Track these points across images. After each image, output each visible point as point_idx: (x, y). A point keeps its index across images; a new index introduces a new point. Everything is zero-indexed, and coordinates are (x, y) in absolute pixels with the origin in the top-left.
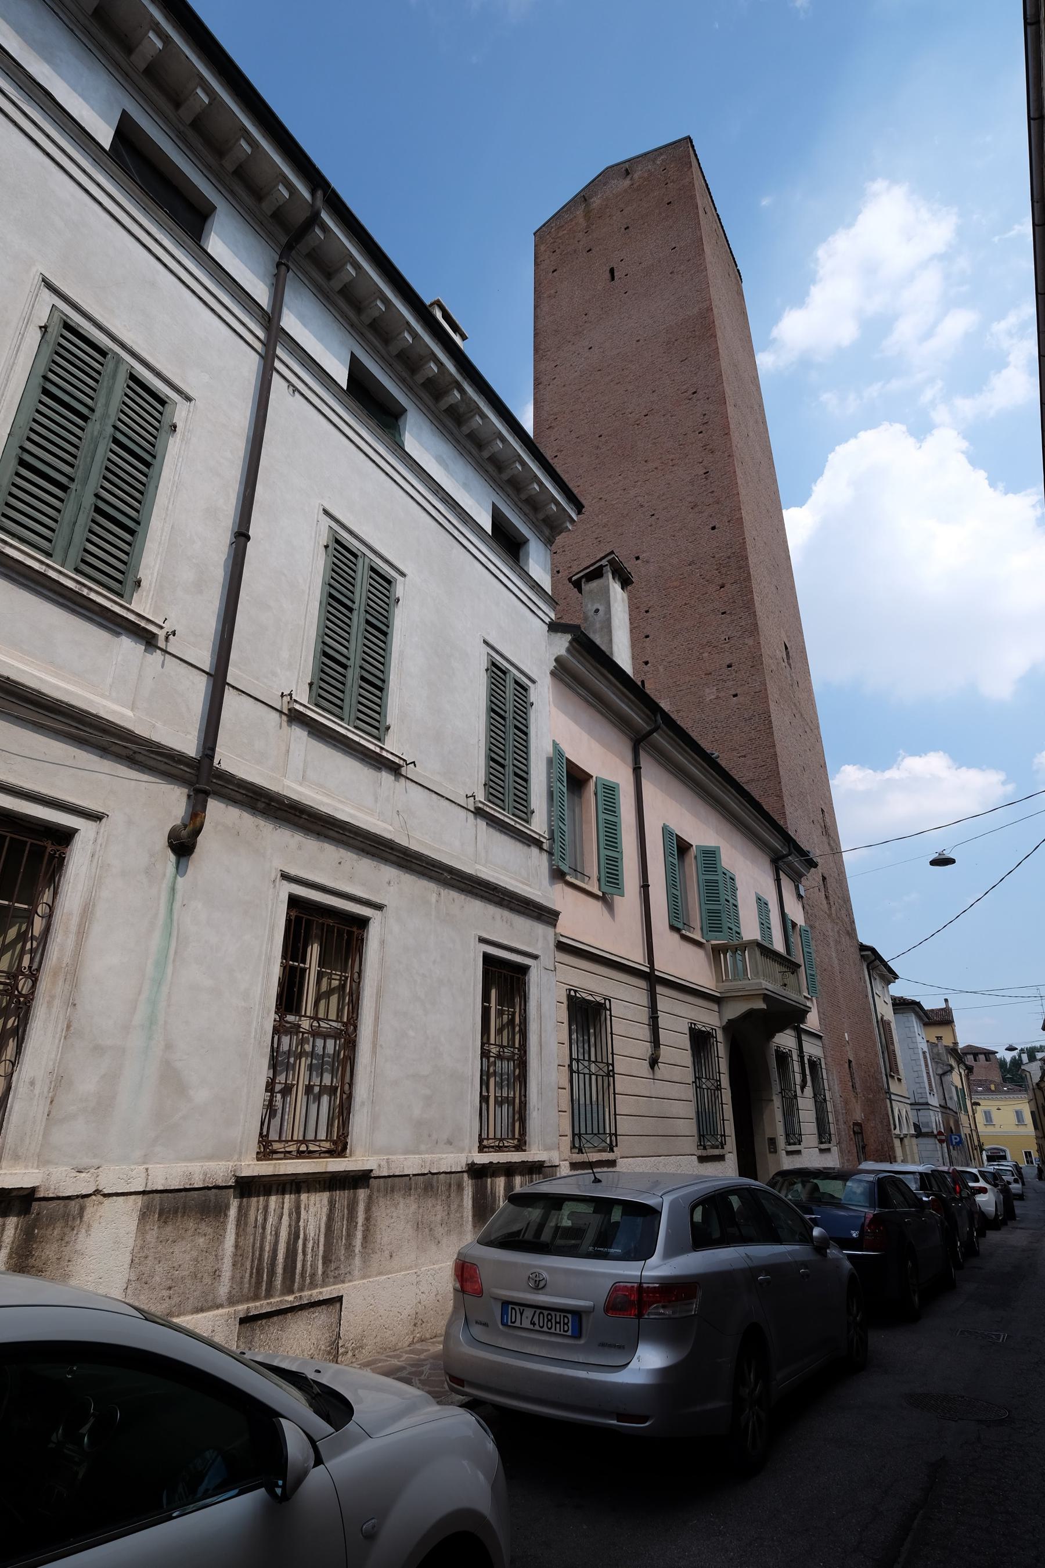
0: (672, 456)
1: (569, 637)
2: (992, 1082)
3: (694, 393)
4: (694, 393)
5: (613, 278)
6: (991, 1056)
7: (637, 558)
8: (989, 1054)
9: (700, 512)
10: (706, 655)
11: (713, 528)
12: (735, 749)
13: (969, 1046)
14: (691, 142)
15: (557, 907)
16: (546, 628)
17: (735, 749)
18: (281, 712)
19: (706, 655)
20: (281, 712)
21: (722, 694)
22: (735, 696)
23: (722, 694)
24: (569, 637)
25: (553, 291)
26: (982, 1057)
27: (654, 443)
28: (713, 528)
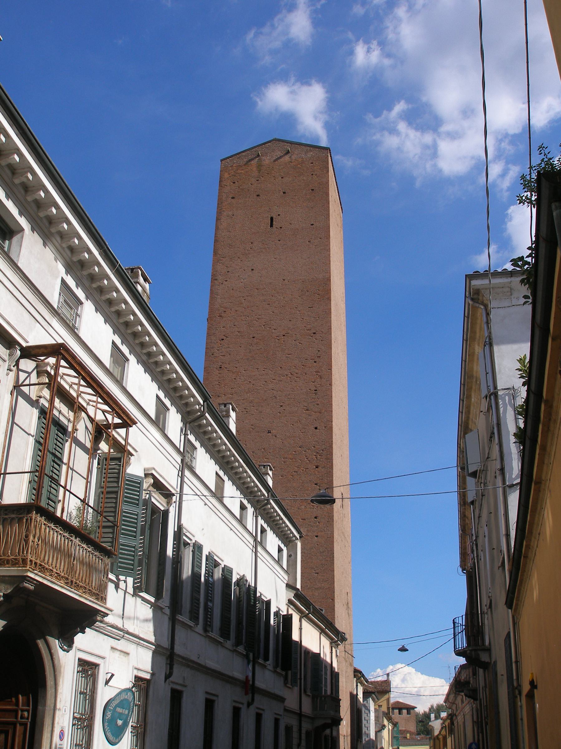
0: (297, 371)
1: (295, 592)
2: (408, 732)
3: (314, 333)
4: (314, 333)
5: (272, 225)
6: (412, 711)
7: (269, 432)
8: (410, 709)
9: (309, 415)
10: (303, 507)
11: (316, 428)
12: (313, 568)
13: (398, 702)
14: (330, 150)
15: (285, 697)
16: (285, 585)
17: (313, 568)
18: (71, 492)
19: (303, 507)
20: (71, 492)
21: (310, 534)
22: (317, 536)
23: (310, 534)
24: (295, 592)
25: (230, 213)
26: (405, 711)
27: (287, 357)
28: (316, 428)
